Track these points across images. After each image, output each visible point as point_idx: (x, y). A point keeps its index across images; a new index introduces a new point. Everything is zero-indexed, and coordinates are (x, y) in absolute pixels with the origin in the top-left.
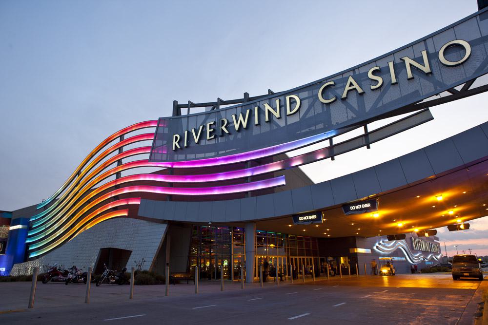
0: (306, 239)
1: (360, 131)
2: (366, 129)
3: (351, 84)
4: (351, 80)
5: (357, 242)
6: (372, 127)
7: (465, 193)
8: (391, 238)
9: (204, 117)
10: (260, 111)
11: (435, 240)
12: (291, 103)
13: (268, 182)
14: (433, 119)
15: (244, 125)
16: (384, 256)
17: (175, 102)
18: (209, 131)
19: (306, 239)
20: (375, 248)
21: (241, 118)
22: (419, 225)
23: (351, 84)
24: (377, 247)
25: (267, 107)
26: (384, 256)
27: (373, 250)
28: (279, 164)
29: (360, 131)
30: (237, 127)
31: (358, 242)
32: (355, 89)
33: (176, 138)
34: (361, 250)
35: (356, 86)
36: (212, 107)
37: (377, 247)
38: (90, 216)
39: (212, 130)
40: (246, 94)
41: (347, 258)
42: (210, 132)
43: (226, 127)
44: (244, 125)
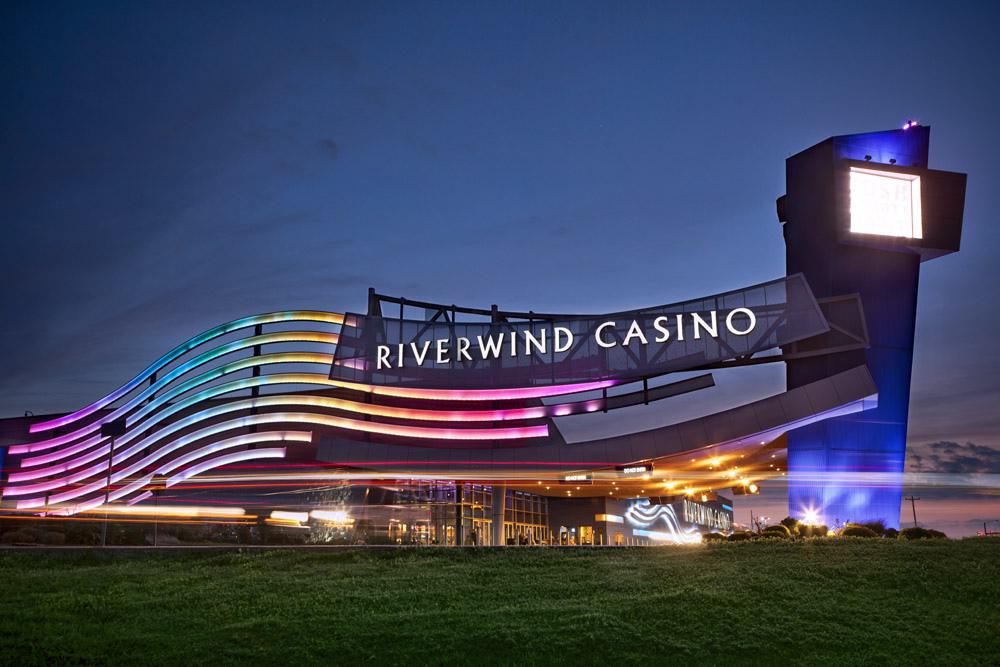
0: (535, 498)
1: (638, 386)
2: (645, 384)
3: (635, 331)
4: (635, 325)
5: (607, 504)
6: (653, 383)
7: (742, 456)
8: (654, 501)
9: (421, 327)
10: (521, 340)
11: (724, 506)
12: (560, 337)
13: (525, 431)
14: (714, 385)
15: (496, 353)
16: (639, 528)
17: (371, 290)
18: (440, 351)
19: (535, 498)
20: (628, 515)
21: (491, 342)
22: (695, 485)
23: (635, 331)
24: (632, 515)
25: (529, 336)
26: (639, 528)
27: (625, 518)
28: (539, 410)
29: (638, 386)
30: (485, 354)
31: (608, 506)
32: (638, 337)
33: (384, 352)
34: (610, 518)
35: (640, 334)
36: (437, 311)
37: (632, 515)
38: (146, 442)
39: (445, 351)
40: (494, 307)
41: (590, 528)
42: (442, 354)
43: (467, 350)
44: (496, 353)
